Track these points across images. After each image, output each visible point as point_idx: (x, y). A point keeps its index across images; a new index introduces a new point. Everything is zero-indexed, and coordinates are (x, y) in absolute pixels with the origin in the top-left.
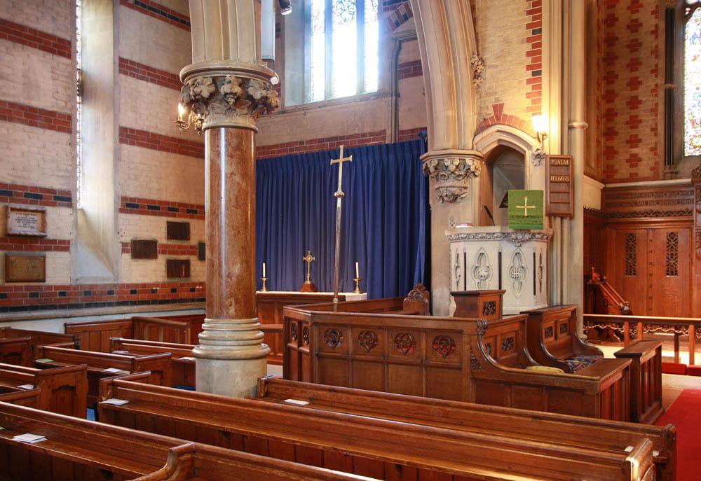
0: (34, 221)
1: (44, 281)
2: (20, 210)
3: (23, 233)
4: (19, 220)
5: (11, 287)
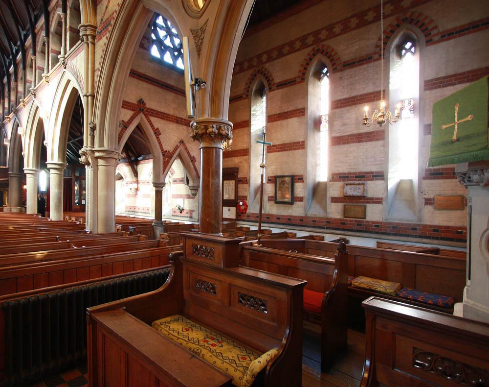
0: (359, 189)
1: (365, 218)
2: (350, 184)
3: (351, 195)
4: (351, 189)
5: (347, 220)
